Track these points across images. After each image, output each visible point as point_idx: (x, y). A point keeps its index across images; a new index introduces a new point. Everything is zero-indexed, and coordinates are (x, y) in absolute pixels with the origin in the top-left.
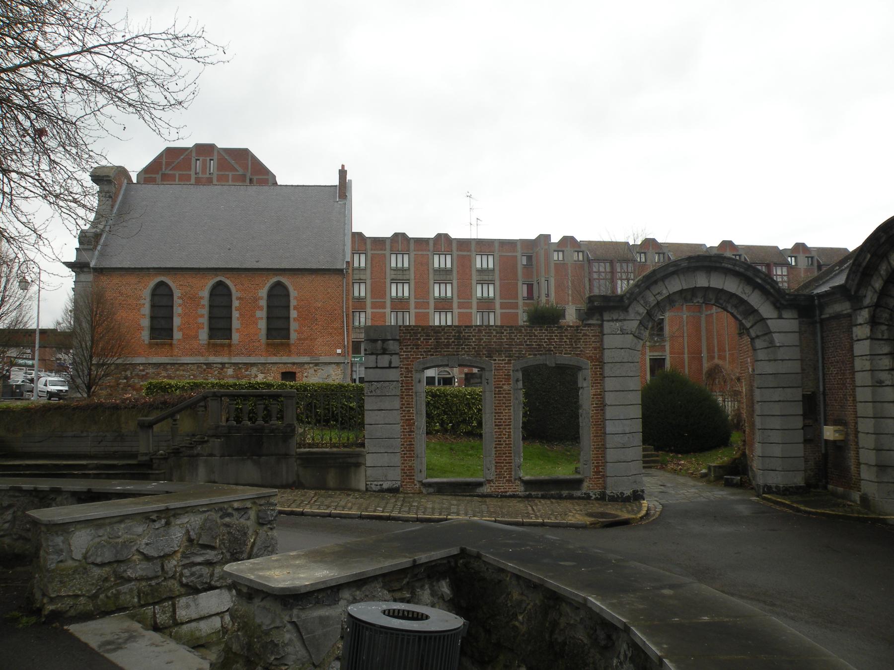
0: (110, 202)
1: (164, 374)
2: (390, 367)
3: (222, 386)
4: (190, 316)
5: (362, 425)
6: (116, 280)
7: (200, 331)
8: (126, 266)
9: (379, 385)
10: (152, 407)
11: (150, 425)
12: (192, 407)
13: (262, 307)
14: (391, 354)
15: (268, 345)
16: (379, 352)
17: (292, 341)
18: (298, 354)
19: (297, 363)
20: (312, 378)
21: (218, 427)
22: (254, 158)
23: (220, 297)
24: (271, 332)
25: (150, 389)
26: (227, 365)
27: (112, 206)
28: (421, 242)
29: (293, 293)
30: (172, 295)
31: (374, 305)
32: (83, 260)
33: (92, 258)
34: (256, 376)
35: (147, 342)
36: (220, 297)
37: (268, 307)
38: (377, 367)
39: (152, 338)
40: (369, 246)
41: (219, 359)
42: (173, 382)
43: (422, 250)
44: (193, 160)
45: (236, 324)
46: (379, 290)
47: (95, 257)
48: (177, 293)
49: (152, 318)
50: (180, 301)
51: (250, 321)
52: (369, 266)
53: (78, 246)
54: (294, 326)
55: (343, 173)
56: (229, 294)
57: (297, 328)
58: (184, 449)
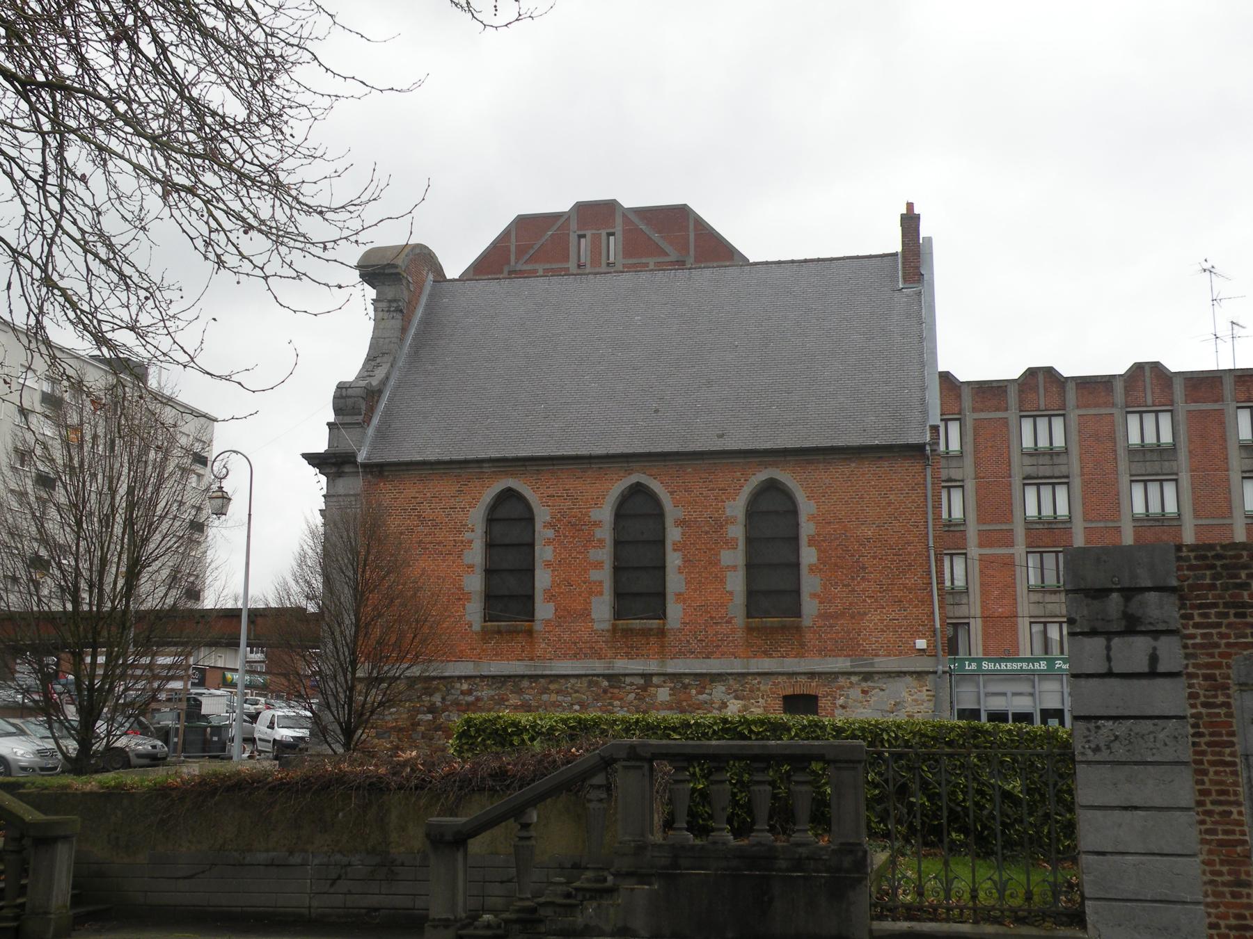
0: (397, 323)
1: (514, 700)
2: (1153, 674)
3: (650, 729)
4: (572, 570)
5: (1071, 855)
6: (410, 490)
7: (593, 599)
8: (432, 458)
9: (1121, 729)
10: (467, 786)
11: (460, 840)
12: (573, 786)
13: (735, 540)
14: (1156, 634)
15: (750, 629)
16: (1115, 627)
17: (807, 621)
18: (823, 652)
19: (820, 674)
20: (854, 708)
21: (641, 849)
22: (700, 223)
23: (639, 519)
24: (756, 599)
25: (469, 735)
26: (655, 680)
27: (404, 330)
28: (1094, 387)
29: (806, 507)
30: (530, 519)
31: (986, 539)
32: (342, 448)
33: (360, 443)
34: (724, 705)
35: (477, 627)
36: (639, 519)
37: (749, 541)
38: (1110, 674)
39: (488, 617)
40: (967, 402)
41: (636, 666)
42: (524, 718)
43: (1097, 406)
44: (573, 238)
45: (675, 582)
46: (995, 506)
47: (368, 441)
48: (542, 515)
49: (489, 572)
50: (550, 533)
51: (706, 577)
52: (969, 448)
53: (331, 418)
54: (810, 584)
55: (910, 222)
56: (660, 515)
57: (819, 589)
58: (549, 912)
